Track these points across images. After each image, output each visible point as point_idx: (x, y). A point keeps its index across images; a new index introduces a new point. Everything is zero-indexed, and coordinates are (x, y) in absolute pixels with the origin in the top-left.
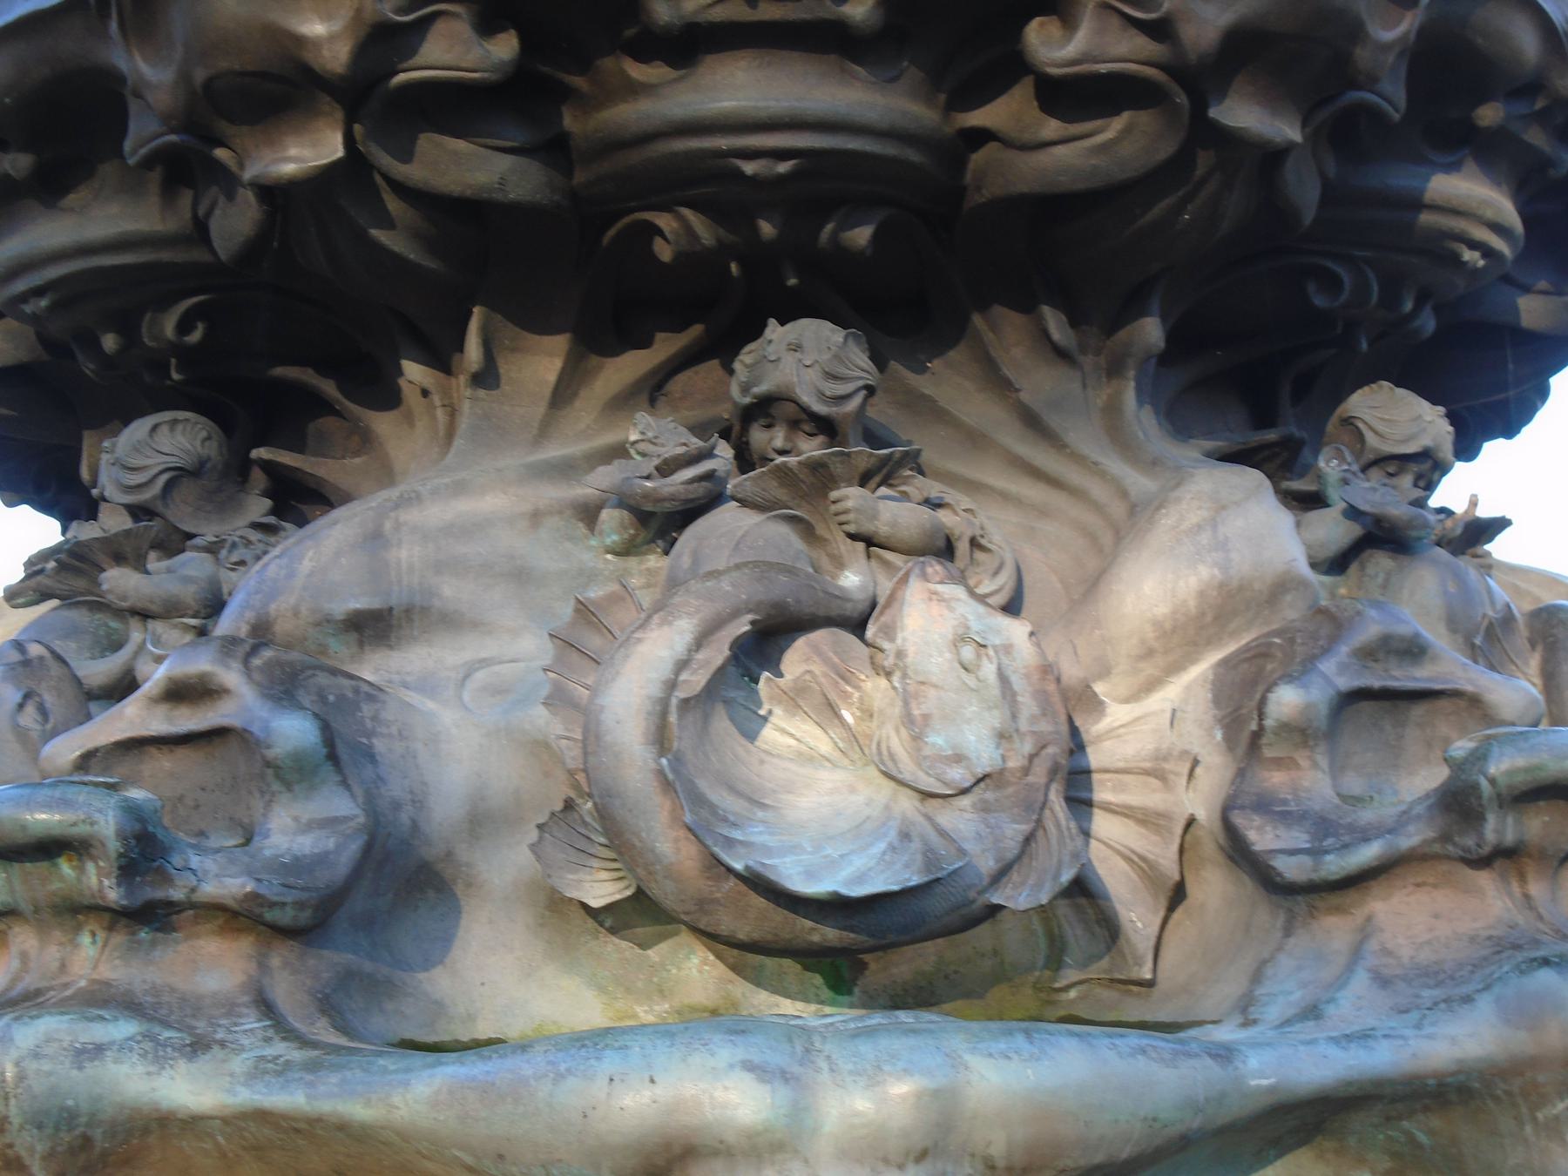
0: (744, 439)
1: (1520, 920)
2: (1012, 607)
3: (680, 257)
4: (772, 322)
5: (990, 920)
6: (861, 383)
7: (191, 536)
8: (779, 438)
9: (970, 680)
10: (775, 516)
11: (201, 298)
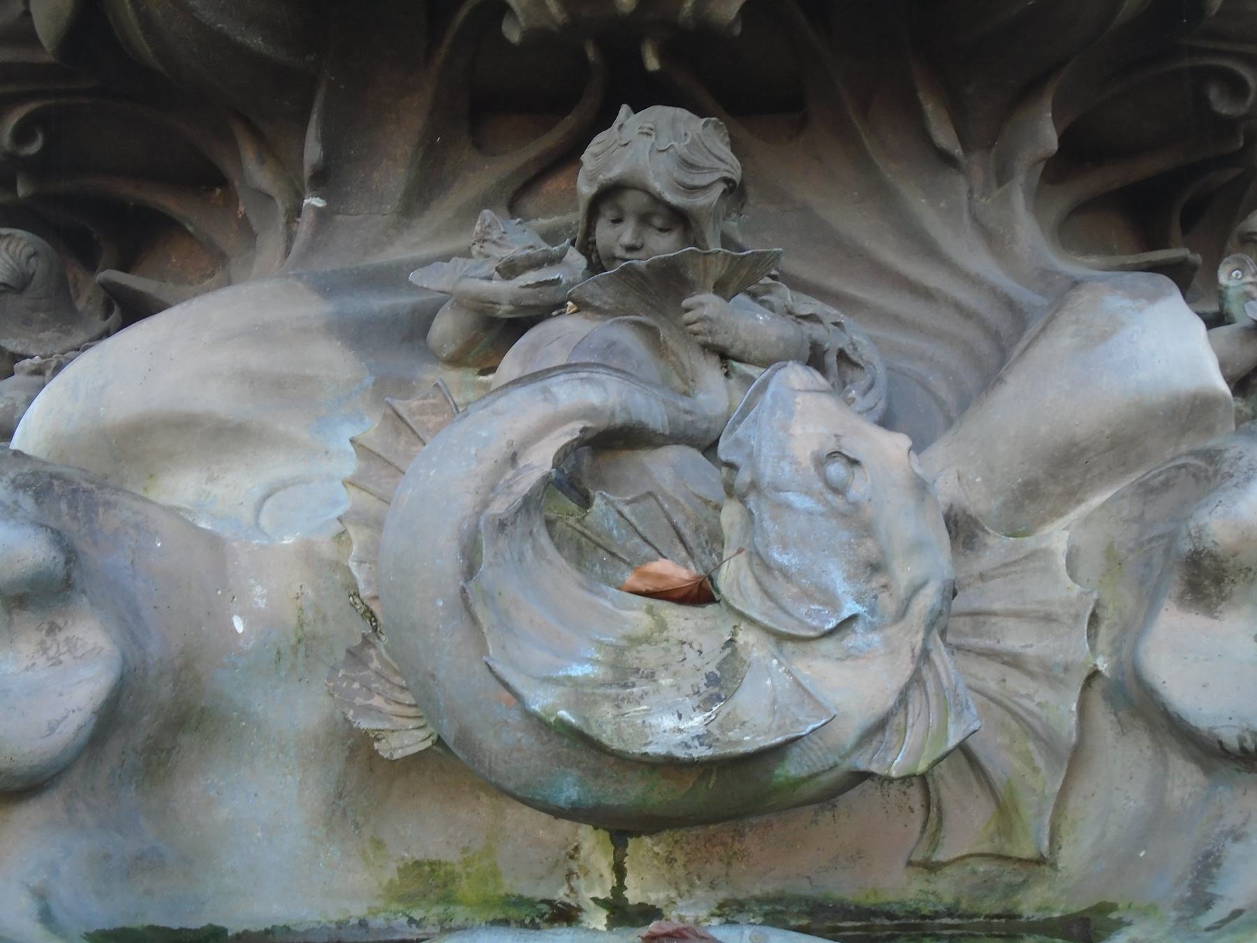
0: (590, 239)
1: (487, 775)
2: (887, 422)
3: (526, 35)
4: (625, 109)
5: (552, 817)
6: (717, 176)
7: (17, 357)
8: (626, 233)
9: (837, 501)
10: (616, 321)
11: (33, 105)
